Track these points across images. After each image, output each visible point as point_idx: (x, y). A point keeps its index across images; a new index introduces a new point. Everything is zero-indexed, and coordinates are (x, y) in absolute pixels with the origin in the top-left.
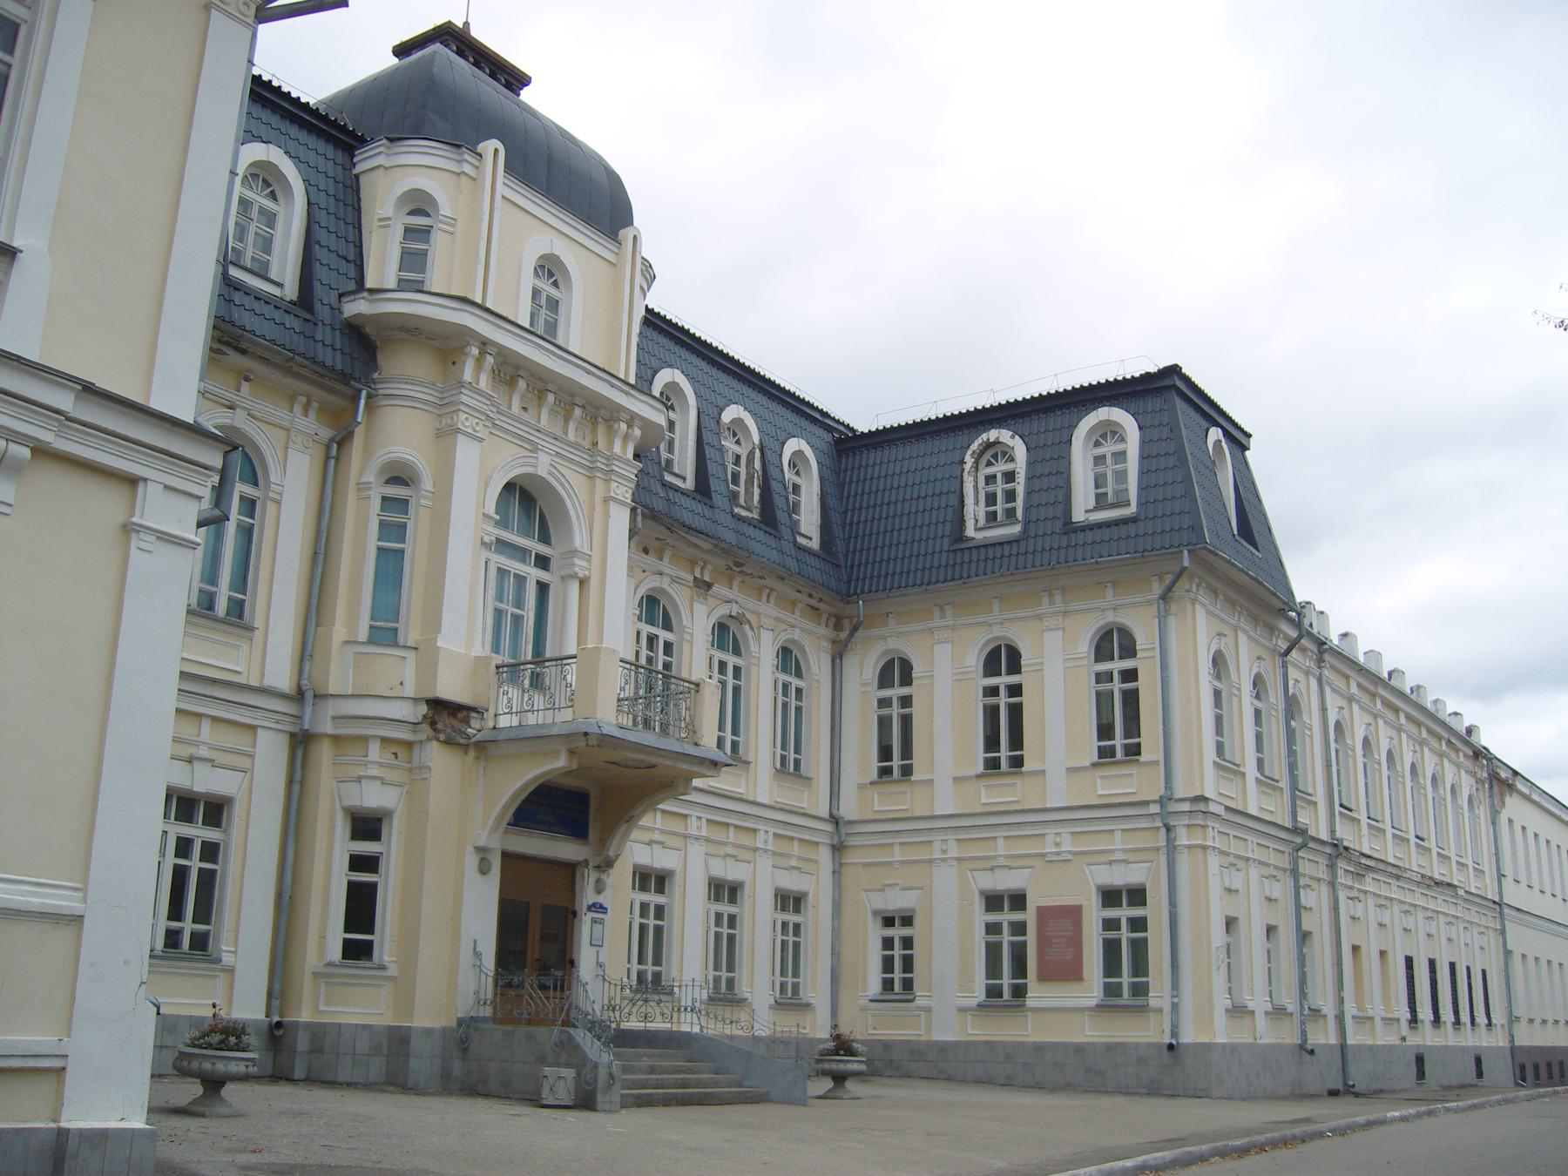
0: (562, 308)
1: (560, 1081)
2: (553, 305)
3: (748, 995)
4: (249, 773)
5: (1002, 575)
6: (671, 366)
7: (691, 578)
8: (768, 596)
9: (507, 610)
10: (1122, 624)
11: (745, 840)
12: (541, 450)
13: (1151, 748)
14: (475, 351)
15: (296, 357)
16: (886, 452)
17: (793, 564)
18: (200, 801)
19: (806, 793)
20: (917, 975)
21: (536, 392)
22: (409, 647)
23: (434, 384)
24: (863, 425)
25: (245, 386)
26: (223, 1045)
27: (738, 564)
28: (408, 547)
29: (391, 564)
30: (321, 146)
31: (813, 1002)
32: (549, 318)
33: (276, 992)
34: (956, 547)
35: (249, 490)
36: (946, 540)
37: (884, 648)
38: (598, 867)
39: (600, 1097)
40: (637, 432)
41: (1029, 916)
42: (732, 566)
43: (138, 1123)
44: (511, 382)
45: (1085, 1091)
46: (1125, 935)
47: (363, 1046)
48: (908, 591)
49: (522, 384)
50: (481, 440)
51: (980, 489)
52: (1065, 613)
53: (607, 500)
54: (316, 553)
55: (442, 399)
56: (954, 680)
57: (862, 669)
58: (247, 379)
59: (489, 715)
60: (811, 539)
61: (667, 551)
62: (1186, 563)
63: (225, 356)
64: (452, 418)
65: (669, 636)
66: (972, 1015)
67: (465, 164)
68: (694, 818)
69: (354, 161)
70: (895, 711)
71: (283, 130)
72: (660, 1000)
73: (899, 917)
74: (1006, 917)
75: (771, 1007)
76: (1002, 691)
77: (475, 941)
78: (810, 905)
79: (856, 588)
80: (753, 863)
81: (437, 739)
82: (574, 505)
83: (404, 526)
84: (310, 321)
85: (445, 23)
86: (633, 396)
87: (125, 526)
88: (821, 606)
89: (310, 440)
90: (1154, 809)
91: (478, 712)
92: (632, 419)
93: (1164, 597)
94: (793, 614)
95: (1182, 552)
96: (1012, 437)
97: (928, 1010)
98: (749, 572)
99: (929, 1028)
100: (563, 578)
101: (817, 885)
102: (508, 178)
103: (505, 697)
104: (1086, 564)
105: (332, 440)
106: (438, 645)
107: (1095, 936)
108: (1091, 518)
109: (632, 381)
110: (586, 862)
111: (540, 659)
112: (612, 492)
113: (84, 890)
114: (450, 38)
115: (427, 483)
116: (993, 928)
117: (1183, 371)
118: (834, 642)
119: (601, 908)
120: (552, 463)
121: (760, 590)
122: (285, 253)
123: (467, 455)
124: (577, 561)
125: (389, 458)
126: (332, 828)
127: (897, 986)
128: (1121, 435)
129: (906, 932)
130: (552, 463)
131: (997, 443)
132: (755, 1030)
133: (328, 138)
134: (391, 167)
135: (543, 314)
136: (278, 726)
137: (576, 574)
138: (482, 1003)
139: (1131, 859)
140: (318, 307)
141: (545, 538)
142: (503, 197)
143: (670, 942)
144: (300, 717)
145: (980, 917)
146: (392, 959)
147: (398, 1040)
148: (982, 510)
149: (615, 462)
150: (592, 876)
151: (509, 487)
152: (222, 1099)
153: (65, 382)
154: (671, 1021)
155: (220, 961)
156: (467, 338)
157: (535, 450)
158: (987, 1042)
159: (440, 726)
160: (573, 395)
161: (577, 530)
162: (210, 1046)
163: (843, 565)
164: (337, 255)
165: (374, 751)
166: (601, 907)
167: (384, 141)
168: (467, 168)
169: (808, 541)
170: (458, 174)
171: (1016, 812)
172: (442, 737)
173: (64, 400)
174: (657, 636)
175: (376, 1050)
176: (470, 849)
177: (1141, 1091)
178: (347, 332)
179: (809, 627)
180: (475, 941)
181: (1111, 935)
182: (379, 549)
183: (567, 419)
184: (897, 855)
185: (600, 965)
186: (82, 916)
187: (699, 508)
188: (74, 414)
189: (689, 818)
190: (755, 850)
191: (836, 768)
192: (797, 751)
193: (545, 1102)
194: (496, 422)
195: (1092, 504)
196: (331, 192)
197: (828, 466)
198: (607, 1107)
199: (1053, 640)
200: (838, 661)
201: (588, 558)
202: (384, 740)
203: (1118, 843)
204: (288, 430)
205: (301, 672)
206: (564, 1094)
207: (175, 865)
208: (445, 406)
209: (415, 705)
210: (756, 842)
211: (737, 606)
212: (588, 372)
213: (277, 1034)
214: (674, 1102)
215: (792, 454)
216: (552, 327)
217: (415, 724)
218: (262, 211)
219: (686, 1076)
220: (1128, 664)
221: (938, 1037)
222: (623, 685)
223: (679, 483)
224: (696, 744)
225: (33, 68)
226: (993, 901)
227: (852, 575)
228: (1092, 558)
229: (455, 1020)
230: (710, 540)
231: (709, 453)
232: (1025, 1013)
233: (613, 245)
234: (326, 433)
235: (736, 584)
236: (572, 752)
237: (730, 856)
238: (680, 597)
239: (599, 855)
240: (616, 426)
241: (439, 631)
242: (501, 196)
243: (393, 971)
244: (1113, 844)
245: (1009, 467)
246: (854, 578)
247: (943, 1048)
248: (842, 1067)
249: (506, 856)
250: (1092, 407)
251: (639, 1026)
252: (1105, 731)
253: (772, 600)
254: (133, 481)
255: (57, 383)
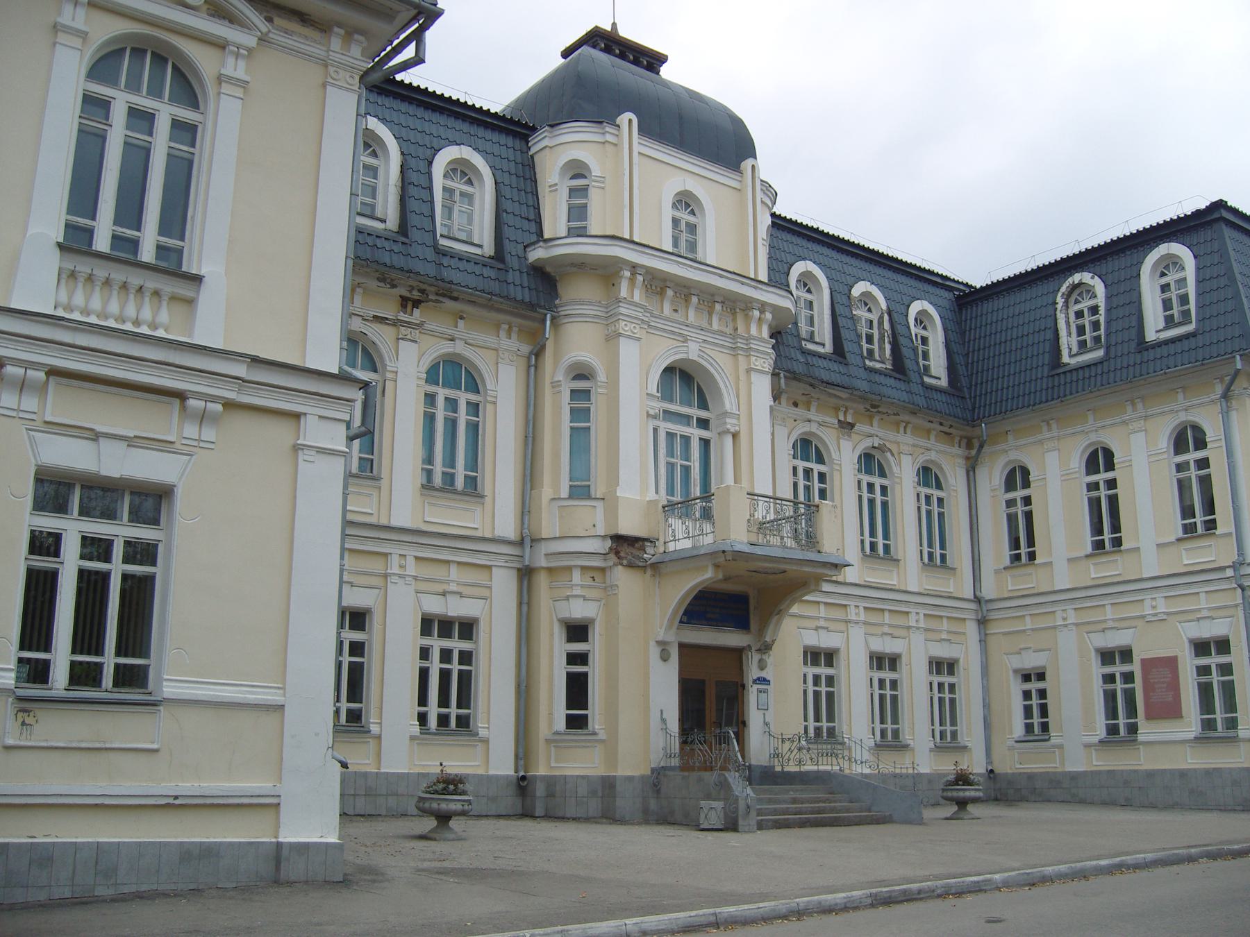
0: (699, 230)
1: (713, 811)
2: (692, 228)
3: (910, 742)
4: (489, 600)
5: (1091, 392)
6: (804, 259)
7: (837, 421)
8: (905, 428)
9: (677, 463)
10: (1194, 422)
11: (900, 621)
12: (690, 340)
13: (1224, 524)
14: (627, 274)
15: (493, 297)
16: (996, 302)
17: (921, 401)
18: (455, 622)
19: (952, 581)
20: (1052, 719)
21: (683, 296)
22: (598, 499)
23: (600, 302)
24: (979, 280)
25: (461, 323)
26: (444, 792)
27: (874, 406)
28: (592, 425)
29: (580, 437)
30: (503, 139)
31: (970, 745)
32: (690, 239)
33: (521, 755)
34: (1054, 372)
35: (473, 397)
36: (1046, 368)
37: (1007, 459)
38: (759, 650)
39: (741, 822)
40: (769, 316)
41: (1136, 667)
42: (869, 408)
43: (333, 839)
44: (661, 293)
45: (1191, 809)
46: (1215, 678)
47: (582, 791)
48: (1019, 412)
49: (670, 293)
50: (639, 339)
51: (1072, 324)
52: (1146, 418)
53: (749, 371)
54: (526, 437)
55: (607, 312)
56: (1062, 481)
57: (991, 477)
58: (461, 318)
59: (660, 544)
60: (940, 379)
61: (813, 403)
62: (1239, 366)
63: (442, 304)
64: (615, 326)
65: (822, 468)
66: (1096, 750)
67: (607, 135)
68: (852, 607)
69: (529, 145)
70: (1020, 509)
71: (472, 133)
72: (809, 748)
73: (1034, 674)
74: (1118, 669)
75: (931, 750)
76: (1102, 485)
77: (662, 711)
78: (961, 669)
79: (979, 414)
80: (907, 639)
81: (622, 564)
82: (722, 378)
83: (589, 409)
84: (502, 269)
85: (593, 28)
86: (761, 289)
87: (294, 446)
88: (951, 430)
89: (514, 355)
90: (1230, 573)
91: (651, 542)
92: (763, 306)
93: (1226, 396)
94: (929, 440)
95: (1234, 357)
96: (1093, 278)
97: (1061, 747)
98: (885, 411)
99: (1062, 763)
100: (719, 434)
101: (967, 652)
102: (641, 139)
103: (670, 528)
104: (1158, 376)
105: (531, 353)
106: (618, 494)
107: (1190, 680)
108: (1161, 337)
109: (763, 276)
110: (749, 647)
111: (707, 495)
112: (752, 364)
113: (283, 689)
114: (598, 39)
115: (602, 376)
116: (1109, 679)
117: (1229, 204)
118: (967, 458)
119: (765, 681)
120: (700, 348)
121: (897, 424)
122: (482, 222)
123: (629, 352)
124: (728, 420)
125: (572, 361)
126: (552, 635)
127: (1037, 729)
128: (1181, 265)
129: (1040, 685)
130: (700, 348)
131: (1080, 284)
132: (880, 767)
133: (508, 132)
134: (553, 147)
135: (684, 236)
136: (507, 564)
137: (728, 430)
138: (668, 756)
139: (1214, 616)
140: (508, 258)
141: (704, 405)
142: (639, 153)
143: (839, 702)
144: (522, 557)
145: (1097, 670)
146: (601, 727)
147: (608, 785)
148: (1074, 340)
149: (752, 341)
150: (756, 657)
151: (669, 370)
152: (450, 829)
153: (238, 358)
154: (817, 764)
155: (478, 734)
156: (620, 265)
157: (686, 341)
158: (1109, 771)
159: (622, 554)
160: (713, 295)
161: (726, 397)
162: (436, 792)
163: (967, 397)
164: (521, 217)
165: (577, 577)
166: (765, 680)
167: (547, 128)
168: (609, 138)
169: (937, 381)
170: (604, 143)
171: (1118, 583)
172: (625, 562)
173: (240, 370)
174: (812, 469)
175: (593, 793)
176: (652, 643)
177: (1238, 808)
178: (532, 273)
179: (942, 449)
180: (662, 711)
181: (1204, 679)
182: (572, 428)
183: (710, 314)
184: (1029, 624)
185: (766, 724)
186: (283, 706)
187: (835, 366)
188: (248, 378)
189: (848, 607)
190: (909, 628)
191: (976, 557)
192: (943, 546)
193: (702, 827)
194: (652, 324)
195: (1161, 325)
196: (513, 171)
197: (951, 319)
198: (746, 829)
199: (1138, 440)
200: (971, 473)
201: (738, 417)
202: (583, 568)
203: (1203, 603)
204: (496, 350)
205: (523, 523)
206: (715, 819)
207: (440, 669)
208: (610, 318)
209: (603, 541)
210: (908, 622)
211: (878, 439)
212: (721, 276)
213: (523, 785)
214: (808, 824)
215: (917, 313)
216: (692, 246)
217: (604, 554)
218: (462, 194)
219: (824, 805)
220: (1201, 454)
221: (1070, 768)
222: (764, 514)
223: (820, 349)
224: (819, 552)
225: (206, 155)
226: (1107, 656)
227: (975, 404)
228: (1162, 370)
229: (650, 770)
230: (846, 390)
231: (842, 322)
232: (1137, 747)
233: (736, 175)
234: (526, 349)
235: (875, 422)
236: (717, 566)
237: (886, 634)
238: (828, 437)
239: (759, 641)
240: (751, 313)
241: (618, 485)
242: (637, 154)
243: (602, 735)
244: (1200, 604)
245: (1092, 302)
246: (977, 406)
247: (1074, 777)
248: (961, 794)
249: (682, 646)
250: (1155, 244)
251: (797, 769)
252: (1187, 511)
253: (909, 430)
254: (297, 416)
255: (235, 360)
